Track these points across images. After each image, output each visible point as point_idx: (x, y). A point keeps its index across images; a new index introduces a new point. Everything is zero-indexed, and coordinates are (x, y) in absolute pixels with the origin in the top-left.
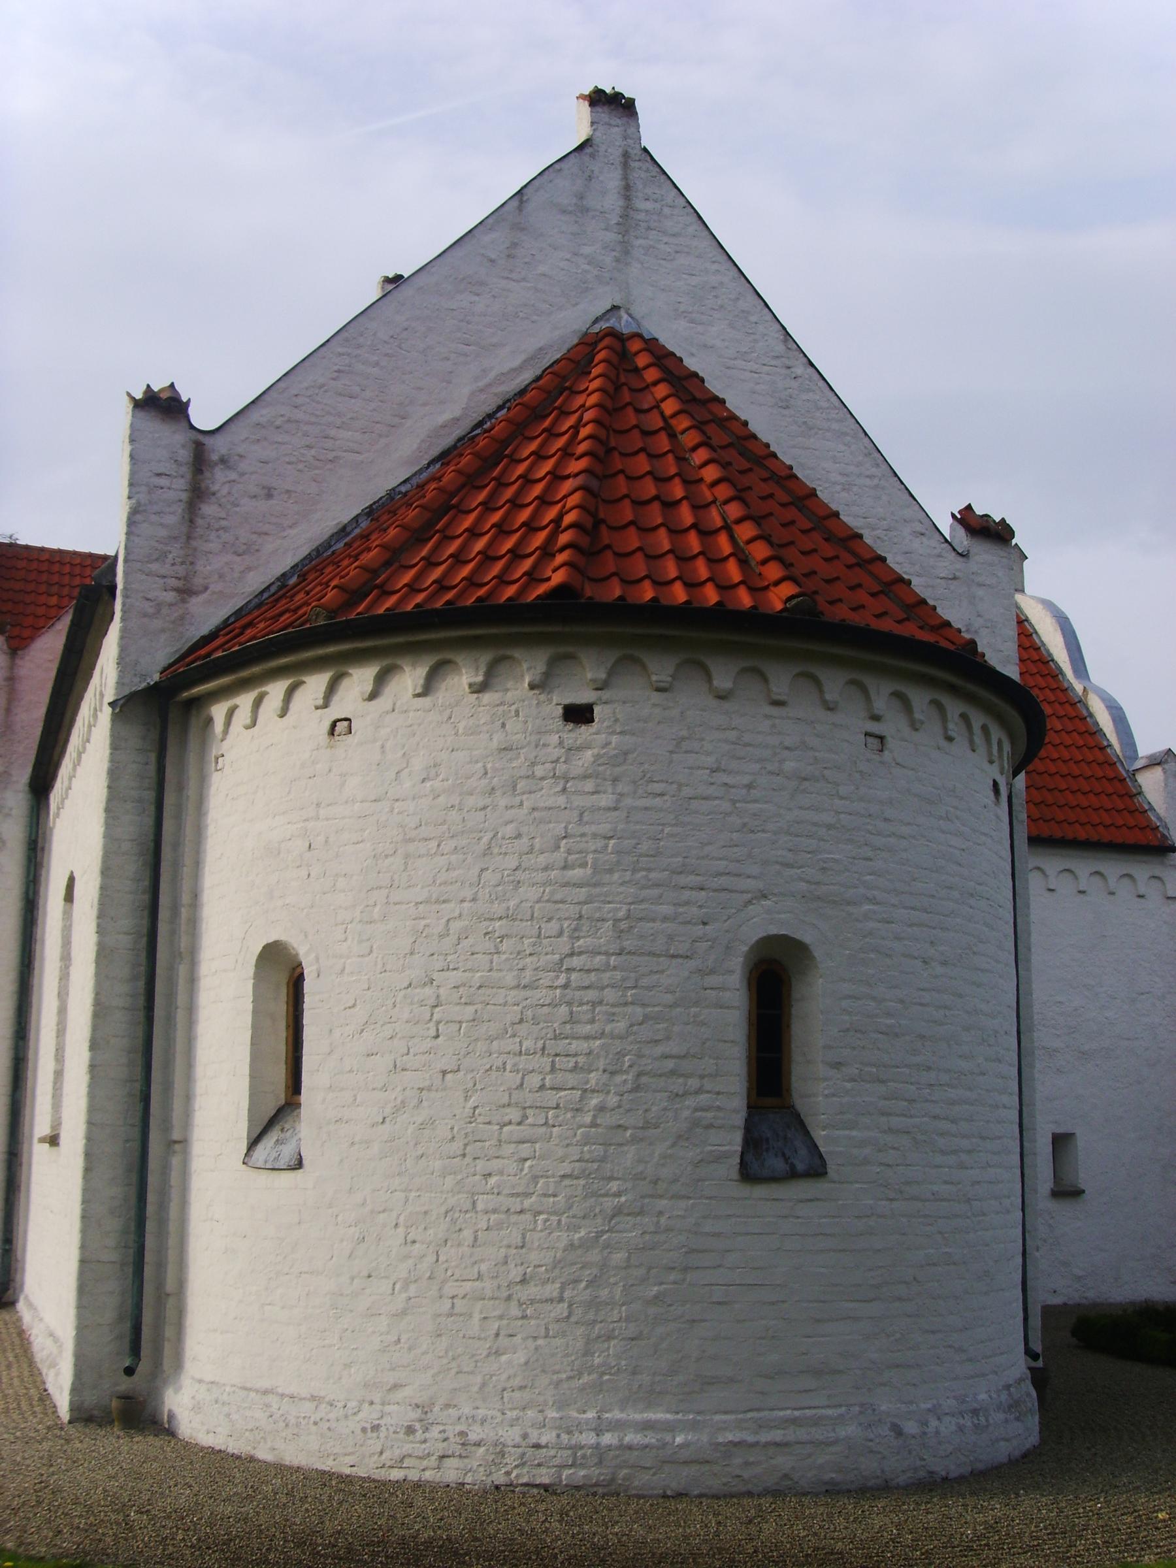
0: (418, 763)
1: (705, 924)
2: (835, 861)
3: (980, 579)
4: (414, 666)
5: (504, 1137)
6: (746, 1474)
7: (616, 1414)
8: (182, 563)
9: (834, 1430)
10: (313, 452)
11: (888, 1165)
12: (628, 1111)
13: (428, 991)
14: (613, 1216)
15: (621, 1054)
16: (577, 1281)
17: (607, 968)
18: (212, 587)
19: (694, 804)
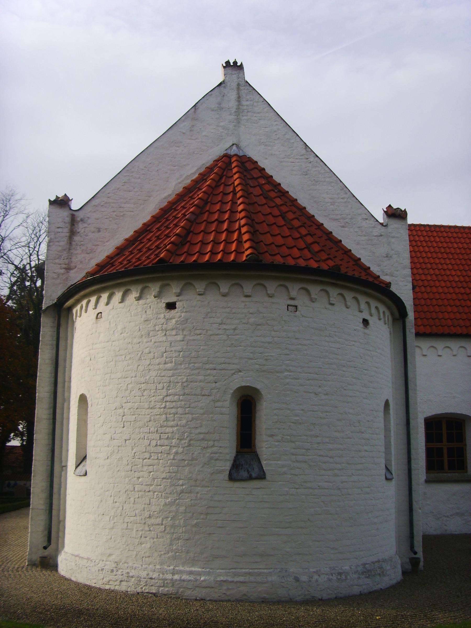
0: (119, 328)
1: (216, 383)
2: (272, 356)
3: (393, 235)
4: (118, 292)
5: (144, 464)
6: (228, 593)
7: (181, 568)
8: (67, 259)
9: (266, 578)
10: (115, 213)
11: (295, 475)
12: (186, 454)
13: (121, 410)
14: (180, 494)
15: (184, 433)
16: (167, 518)
17: (179, 400)
18: (78, 267)
19: (212, 337)
